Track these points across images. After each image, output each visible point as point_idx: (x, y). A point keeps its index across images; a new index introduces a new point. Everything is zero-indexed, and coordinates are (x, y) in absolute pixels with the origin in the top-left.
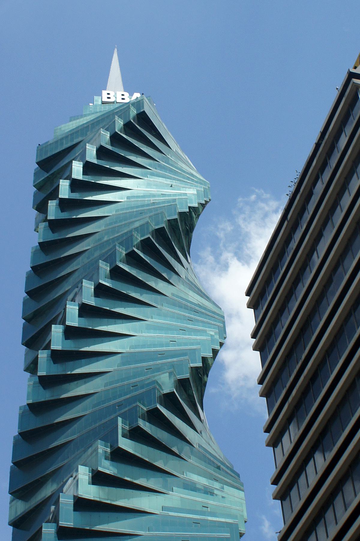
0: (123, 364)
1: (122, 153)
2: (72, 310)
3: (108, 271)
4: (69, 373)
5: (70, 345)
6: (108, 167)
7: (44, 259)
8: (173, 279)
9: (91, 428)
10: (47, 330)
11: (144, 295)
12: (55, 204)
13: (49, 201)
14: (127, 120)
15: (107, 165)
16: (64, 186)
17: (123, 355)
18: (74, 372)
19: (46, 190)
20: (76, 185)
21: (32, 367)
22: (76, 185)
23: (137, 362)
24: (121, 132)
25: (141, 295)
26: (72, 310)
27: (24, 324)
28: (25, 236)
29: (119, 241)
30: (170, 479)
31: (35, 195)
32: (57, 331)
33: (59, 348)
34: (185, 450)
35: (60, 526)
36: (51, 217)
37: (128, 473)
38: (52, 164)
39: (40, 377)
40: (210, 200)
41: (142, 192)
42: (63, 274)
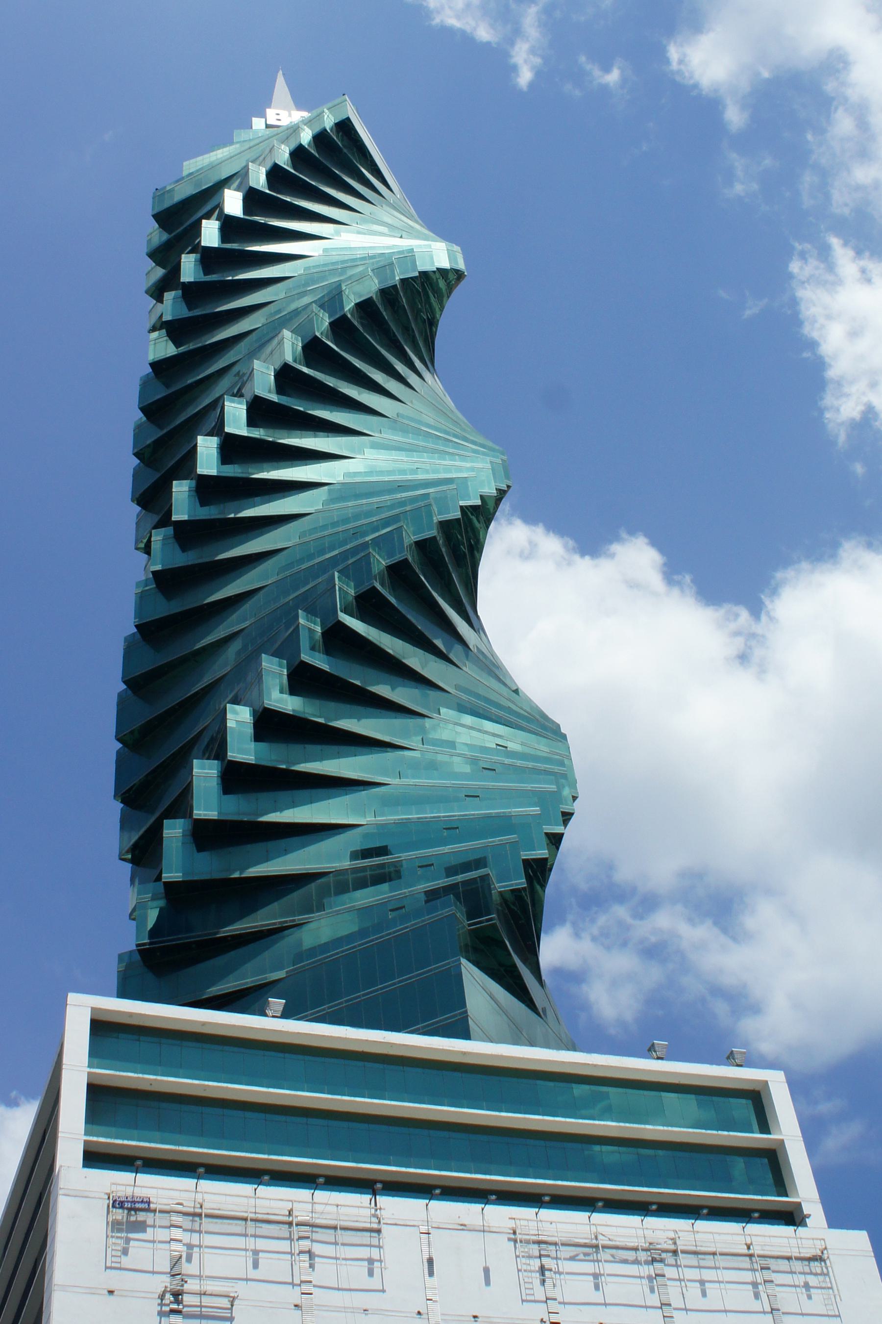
0: (332, 500)
1: (330, 381)
3: (300, 348)
4: (236, 875)
5: (236, 808)
7: (163, 608)
9: (278, 605)
10: (179, 762)
11: (400, 690)
12: (186, 489)
13: (174, 482)
14: (365, 588)
16: (207, 449)
17: (331, 487)
18: (293, 768)
19: (161, 456)
20: (232, 449)
22: (232, 449)
23: (357, 496)
24: (327, 338)
25: (393, 689)
27: (118, 752)
28: (110, 571)
29: (340, 567)
30: (433, 694)
31: (136, 474)
32: (205, 773)
33: (212, 814)
36: (173, 874)
37: (356, 675)
38: (177, 221)
39: (168, 885)
40: (509, 487)
41: (379, 459)
42: (207, 401)
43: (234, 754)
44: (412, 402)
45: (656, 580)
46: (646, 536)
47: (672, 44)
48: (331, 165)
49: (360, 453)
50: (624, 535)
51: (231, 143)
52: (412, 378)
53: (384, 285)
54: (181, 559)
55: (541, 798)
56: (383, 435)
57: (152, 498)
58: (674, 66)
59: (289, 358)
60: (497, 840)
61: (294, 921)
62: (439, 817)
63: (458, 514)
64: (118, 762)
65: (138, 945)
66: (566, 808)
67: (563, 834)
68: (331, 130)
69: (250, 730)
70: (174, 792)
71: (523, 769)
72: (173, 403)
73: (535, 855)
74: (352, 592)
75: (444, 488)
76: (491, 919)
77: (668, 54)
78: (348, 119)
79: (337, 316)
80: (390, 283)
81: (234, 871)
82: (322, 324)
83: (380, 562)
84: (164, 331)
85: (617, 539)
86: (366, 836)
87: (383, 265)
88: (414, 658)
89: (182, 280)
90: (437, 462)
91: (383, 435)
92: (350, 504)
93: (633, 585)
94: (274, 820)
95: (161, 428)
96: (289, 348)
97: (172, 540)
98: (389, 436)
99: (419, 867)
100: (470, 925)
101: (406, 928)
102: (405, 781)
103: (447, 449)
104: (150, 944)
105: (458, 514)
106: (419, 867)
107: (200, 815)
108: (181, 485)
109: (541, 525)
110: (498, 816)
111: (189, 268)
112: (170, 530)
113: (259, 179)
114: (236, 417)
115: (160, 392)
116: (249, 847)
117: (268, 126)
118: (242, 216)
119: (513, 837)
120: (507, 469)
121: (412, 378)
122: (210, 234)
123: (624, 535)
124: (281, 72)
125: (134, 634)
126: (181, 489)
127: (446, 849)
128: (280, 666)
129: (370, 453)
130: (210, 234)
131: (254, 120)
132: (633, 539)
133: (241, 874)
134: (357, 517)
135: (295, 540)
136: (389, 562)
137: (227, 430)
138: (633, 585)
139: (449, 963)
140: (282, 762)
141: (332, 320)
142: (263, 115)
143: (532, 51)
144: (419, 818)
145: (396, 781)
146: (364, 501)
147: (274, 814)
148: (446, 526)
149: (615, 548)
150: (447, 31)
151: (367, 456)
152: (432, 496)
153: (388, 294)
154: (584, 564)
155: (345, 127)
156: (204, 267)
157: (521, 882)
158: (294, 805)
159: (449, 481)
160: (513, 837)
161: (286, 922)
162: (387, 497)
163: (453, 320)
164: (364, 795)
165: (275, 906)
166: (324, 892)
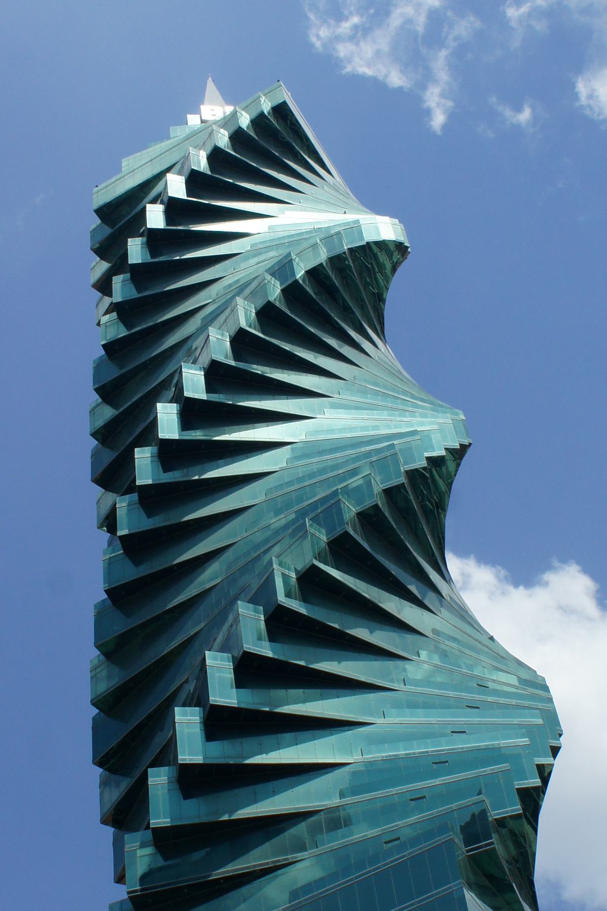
2: (219, 667)
4: (226, 817)
5: (221, 752)
6: (302, 663)
7: (130, 572)
8: (430, 599)
10: (161, 717)
13: (129, 240)
14: (338, 532)
15: (299, 657)
18: (234, 817)
20: (192, 412)
21: (126, 814)
22: (219, 723)
23: (321, 453)
25: (371, 632)
26: (219, 667)
27: (94, 719)
30: (410, 637)
31: (95, 455)
32: (187, 721)
33: (198, 759)
34: (430, 599)
35: (212, 705)
41: (341, 420)
43: (216, 698)
44: (367, 366)
45: (590, 606)
46: (578, 563)
47: (580, 79)
48: (269, 150)
49: (320, 414)
50: (556, 563)
51: (169, 138)
52: (366, 345)
53: (332, 254)
54: (146, 523)
55: (529, 730)
56: (341, 396)
57: (113, 475)
58: (583, 100)
59: (243, 324)
60: (488, 769)
61: (287, 859)
62: (427, 752)
63: (424, 463)
64: (94, 728)
65: (129, 893)
66: (554, 743)
67: (553, 765)
68: (269, 113)
69: (230, 675)
70: (159, 740)
71: (506, 706)
72: (131, 371)
73: (528, 783)
74: (324, 538)
75: (409, 439)
76: (492, 843)
77: (577, 90)
78: (284, 103)
79: (290, 282)
80: (338, 251)
81: (225, 813)
82: (275, 291)
83: (350, 509)
84: (115, 314)
85: (549, 568)
86: (354, 774)
87: (330, 237)
88: (391, 604)
89: (130, 261)
90: (399, 419)
91: (341, 396)
92: (314, 460)
93: (566, 610)
94: (260, 762)
95: (188, 196)
96: (245, 315)
97: (137, 506)
98: (346, 396)
99: (411, 800)
100: (468, 851)
101: (404, 856)
102: (389, 720)
103: (406, 408)
104: (142, 890)
105: (424, 463)
106: (411, 800)
107: (185, 760)
108: (143, 452)
109: (472, 556)
110: (486, 749)
111: (136, 250)
112: (135, 496)
113: (201, 163)
114: (194, 382)
115: (113, 372)
116: (236, 791)
117: (203, 121)
118: (185, 197)
119: (505, 766)
120: (468, 426)
121: (366, 345)
122: (155, 217)
123: (556, 563)
124: (210, 79)
125: (103, 601)
126: (143, 456)
127: (437, 781)
128: (256, 611)
129: (329, 413)
130: (155, 217)
131: (189, 117)
132: (565, 566)
133: (230, 816)
134: (323, 471)
135: (261, 498)
136: (359, 509)
137: (186, 394)
138: (566, 610)
139: (451, 887)
140: (266, 705)
141: (284, 286)
142: (197, 111)
143: (442, 95)
144: (407, 754)
145: (380, 721)
146: (328, 457)
147: (260, 756)
148: (412, 475)
149: (549, 576)
150: (357, 80)
151: (327, 415)
152: (397, 448)
153: (337, 261)
154: (519, 594)
155: (281, 110)
156: (149, 261)
157: (516, 808)
158: (278, 747)
159: (415, 433)
160: (505, 766)
161: (279, 861)
162: (352, 452)
163: (400, 293)
164: (348, 735)
165: (267, 846)
166: (315, 830)
